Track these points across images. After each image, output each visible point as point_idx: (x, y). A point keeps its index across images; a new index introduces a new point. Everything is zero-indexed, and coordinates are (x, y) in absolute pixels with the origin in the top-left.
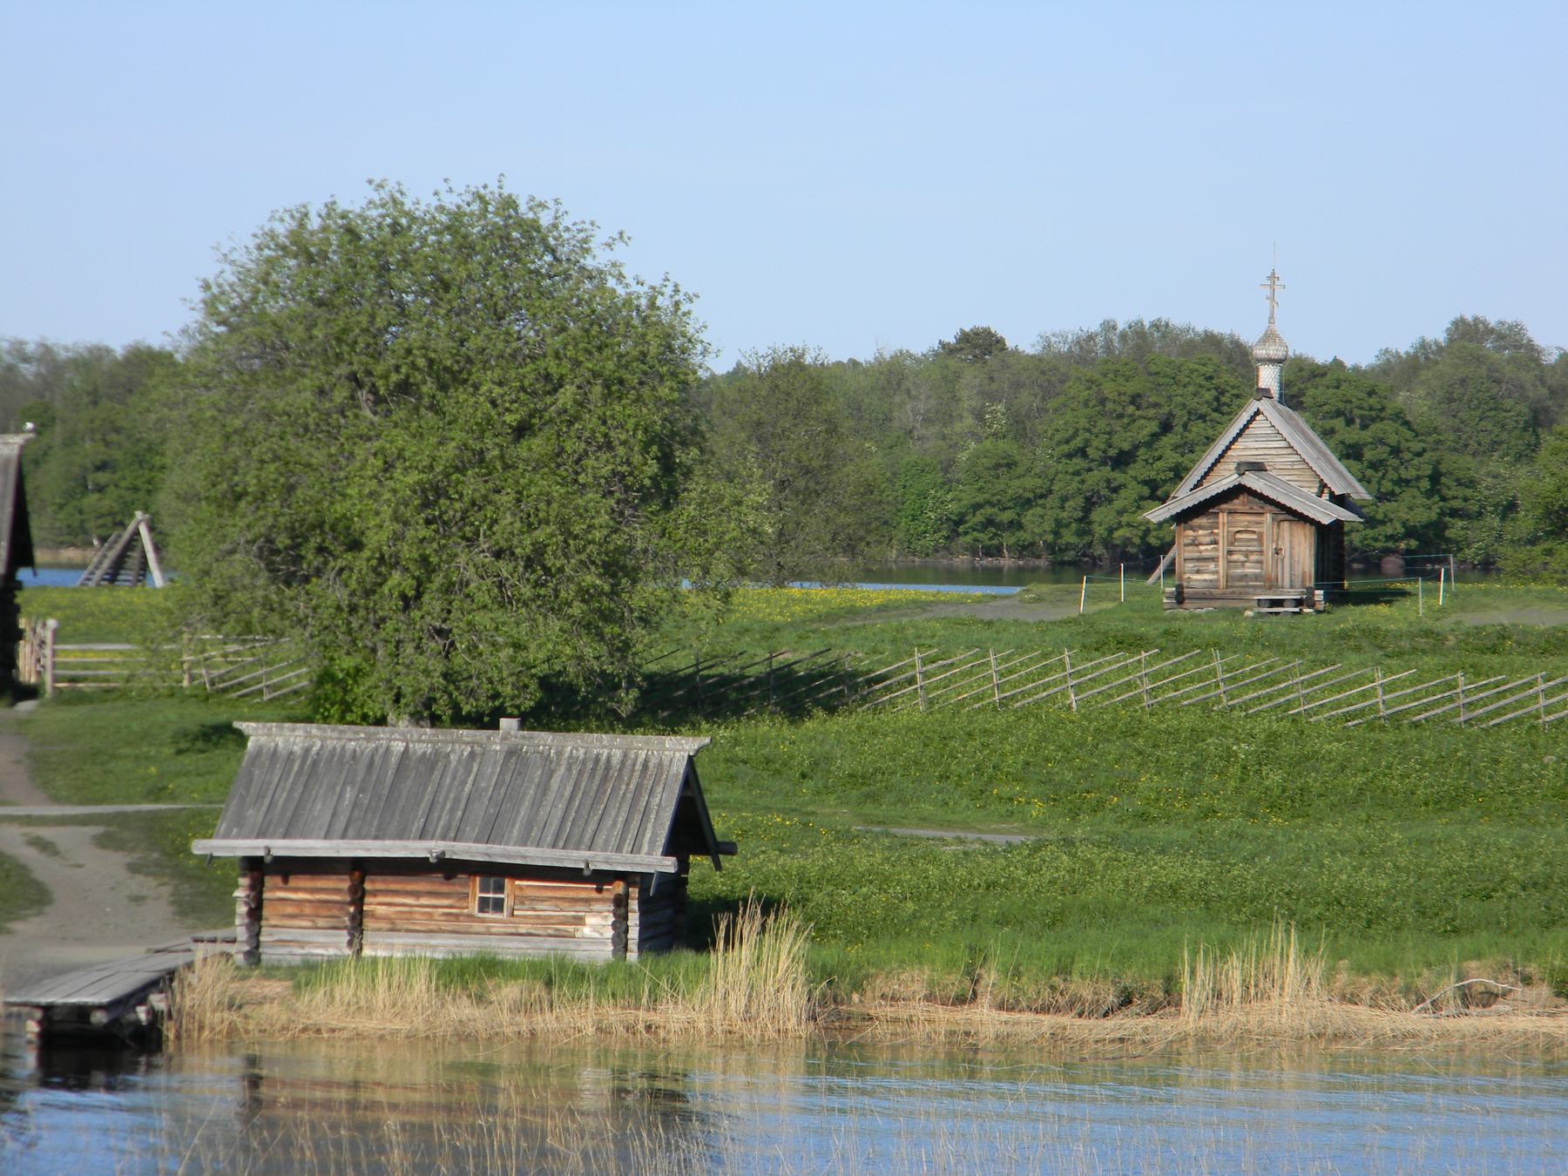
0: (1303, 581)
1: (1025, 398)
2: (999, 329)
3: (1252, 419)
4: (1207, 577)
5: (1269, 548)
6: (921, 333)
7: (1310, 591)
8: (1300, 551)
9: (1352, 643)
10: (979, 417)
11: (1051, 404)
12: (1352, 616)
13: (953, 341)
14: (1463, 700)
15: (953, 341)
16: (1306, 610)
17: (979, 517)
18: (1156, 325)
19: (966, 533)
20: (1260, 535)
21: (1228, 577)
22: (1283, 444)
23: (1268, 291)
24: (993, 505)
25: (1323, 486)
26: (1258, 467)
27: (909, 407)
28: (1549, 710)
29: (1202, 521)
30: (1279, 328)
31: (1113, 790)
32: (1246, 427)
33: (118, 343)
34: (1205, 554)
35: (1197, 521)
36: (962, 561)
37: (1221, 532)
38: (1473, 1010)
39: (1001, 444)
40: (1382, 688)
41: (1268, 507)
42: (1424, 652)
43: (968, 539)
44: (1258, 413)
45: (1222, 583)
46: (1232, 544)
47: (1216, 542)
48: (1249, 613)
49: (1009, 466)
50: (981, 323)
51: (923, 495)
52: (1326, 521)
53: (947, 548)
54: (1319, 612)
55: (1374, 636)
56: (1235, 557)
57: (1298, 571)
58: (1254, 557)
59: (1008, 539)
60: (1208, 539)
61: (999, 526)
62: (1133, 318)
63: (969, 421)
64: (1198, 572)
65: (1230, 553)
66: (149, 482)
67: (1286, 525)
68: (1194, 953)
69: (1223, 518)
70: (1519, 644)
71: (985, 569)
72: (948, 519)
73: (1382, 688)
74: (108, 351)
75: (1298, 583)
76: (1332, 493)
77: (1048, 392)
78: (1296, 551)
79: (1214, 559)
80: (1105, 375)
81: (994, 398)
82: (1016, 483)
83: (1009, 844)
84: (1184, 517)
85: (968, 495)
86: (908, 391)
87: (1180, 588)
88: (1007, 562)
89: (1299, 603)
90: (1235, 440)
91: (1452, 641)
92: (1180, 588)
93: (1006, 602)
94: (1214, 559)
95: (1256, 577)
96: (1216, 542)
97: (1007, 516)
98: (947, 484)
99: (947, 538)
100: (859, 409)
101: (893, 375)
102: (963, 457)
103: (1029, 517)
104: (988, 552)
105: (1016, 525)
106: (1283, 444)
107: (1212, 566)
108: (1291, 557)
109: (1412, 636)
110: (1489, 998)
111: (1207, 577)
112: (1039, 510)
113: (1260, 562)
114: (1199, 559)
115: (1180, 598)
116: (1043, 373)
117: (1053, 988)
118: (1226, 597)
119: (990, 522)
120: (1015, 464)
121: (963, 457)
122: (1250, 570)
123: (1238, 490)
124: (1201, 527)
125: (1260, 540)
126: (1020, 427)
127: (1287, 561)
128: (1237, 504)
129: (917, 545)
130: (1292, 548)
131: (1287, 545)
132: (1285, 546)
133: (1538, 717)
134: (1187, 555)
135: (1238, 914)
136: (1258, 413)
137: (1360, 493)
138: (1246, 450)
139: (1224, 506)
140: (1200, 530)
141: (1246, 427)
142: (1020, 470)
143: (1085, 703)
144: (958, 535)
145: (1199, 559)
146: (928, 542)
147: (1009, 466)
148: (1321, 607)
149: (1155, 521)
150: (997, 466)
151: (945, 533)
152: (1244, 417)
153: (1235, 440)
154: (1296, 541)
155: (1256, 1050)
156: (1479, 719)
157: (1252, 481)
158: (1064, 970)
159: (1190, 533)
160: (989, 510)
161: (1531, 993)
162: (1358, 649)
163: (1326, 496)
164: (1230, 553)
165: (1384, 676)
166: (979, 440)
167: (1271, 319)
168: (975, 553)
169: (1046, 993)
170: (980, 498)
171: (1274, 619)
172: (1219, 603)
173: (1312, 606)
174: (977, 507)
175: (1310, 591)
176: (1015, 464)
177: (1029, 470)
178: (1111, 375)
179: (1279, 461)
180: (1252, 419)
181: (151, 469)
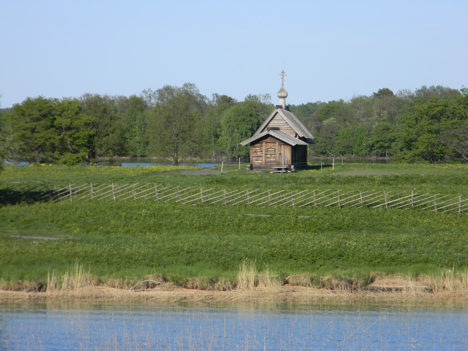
0: (288, 163)
1: (393, 109)
2: (391, 89)
3: (275, 115)
4: (259, 162)
5: (278, 153)
6: (368, 91)
7: (290, 166)
8: (287, 154)
9: (287, 181)
10: (379, 115)
11: (400, 111)
12: (304, 173)
13: (377, 92)
14: (225, 197)
15: (377, 92)
16: (289, 171)
17: (379, 145)
18: (438, 87)
19: (375, 150)
20: (275, 149)
21: (266, 162)
22: (284, 122)
23: (281, 77)
24: (383, 141)
25: (297, 134)
26: (276, 129)
27: (358, 112)
28: (250, 200)
29: (258, 145)
30: (285, 87)
31: (102, 225)
32: (274, 117)
33: (128, 95)
34: (259, 155)
35: (256, 145)
36: (374, 158)
37: (263, 148)
38: (149, 289)
39: (385, 123)
40: (317, 195)
41: (277, 141)
42: (308, 184)
43: (375, 151)
44: (277, 113)
45: (264, 163)
46: (267, 152)
47: (262, 151)
48: (271, 172)
49: (387, 129)
50: (386, 87)
51: (362, 138)
52: (294, 145)
53: (369, 154)
54: (292, 172)
55: (312, 180)
56: (268, 156)
57: (286, 159)
58: (273, 156)
59: (387, 151)
60: (260, 151)
61: (384, 147)
62: (431, 85)
63: (376, 116)
64: (257, 160)
65: (266, 154)
66: (131, 136)
67: (282, 146)
68: (51, 272)
69: (264, 144)
70: (337, 181)
71: (381, 160)
72: (369, 146)
73: (317, 195)
74: (125, 97)
75: (286, 163)
76: (299, 136)
77: (399, 107)
78: (286, 154)
79: (261, 156)
80: (416, 102)
81: (384, 109)
82: (389, 135)
83: (49, 240)
84: (253, 144)
85: (375, 138)
86: (358, 108)
87: (251, 165)
88: (387, 158)
89: (286, 169)
90: (270, 121)
91: (317, 180)
92: (251, 165)
93: (207, 170)
94: (261, 156)
95: (274, 162)
96: (262, 151)
97: (387, 145)
98: (369, 135)
99: (369, 151)
100: (347, 113)
101: (358, 102)
102: (374, 127)
103: (393, 144)
104: (381, 155)
105: (389, 147)
106: (284, 122)
107: (261, 158)
108: (284, 156)
109: (306, 179)
110: (154, 286)
111: (259, 162)
112: (396, 143)
113: (275, 157)
114: (257, 157)
115: (251, 168)
116: (398, 102)
117: (18, 283)
118: (265, 168)
119: (381, 147)
120: (389, 129)
121: (374, 127)
122: (272, 159)
123: (268, 136)
124: (258, 147)
125: (275, 151)
126: (391, 118)
127: (283, 157)
128: (268, 140)
129: (360, 153)
130: (284, 153)
131: (283, 152)
132: (282, 152)
133: (247, 203)
134: (254, 155)
135: (64, 262)
136: (277, 113)
137: (311, 136)
138: (273, 124)
139: (264, 141)
140: (257, 148)
141: (274, 117)
142: (391, 130)
143: (117, 200)
144: (373, 150)
145: (257, 157)
146: (364, 152)
147: (387, 129)
148: (293, 170)
149: (243, 145)
150: (384, 130)
151: (369, 150)
152: (273, 114)
153: (270, 121)
154: (286, 151)
155: (70, 302)
156: (230, 203)
157: (272, 133)
158: (22, 278)
159: (254, 148)
160: (381, 143)
161: (167, 284)
162: (289, 183)
163: (298, 137)
164: (266, 154)
165: (203, 190)
166: (379, 122)
167: (283, 84)
168: (377, 155)
169: (16, 285)
170: (379, 139)
171: (278, 174)
172: (263, 169)
173: (290, 170)
174: (377, 142)
175: (290, 166)
176: (389, 129)
177: (393, 131)
178: (417, 102)
179: (284, 128)
180: (275, 115)
181: (132, 132)
